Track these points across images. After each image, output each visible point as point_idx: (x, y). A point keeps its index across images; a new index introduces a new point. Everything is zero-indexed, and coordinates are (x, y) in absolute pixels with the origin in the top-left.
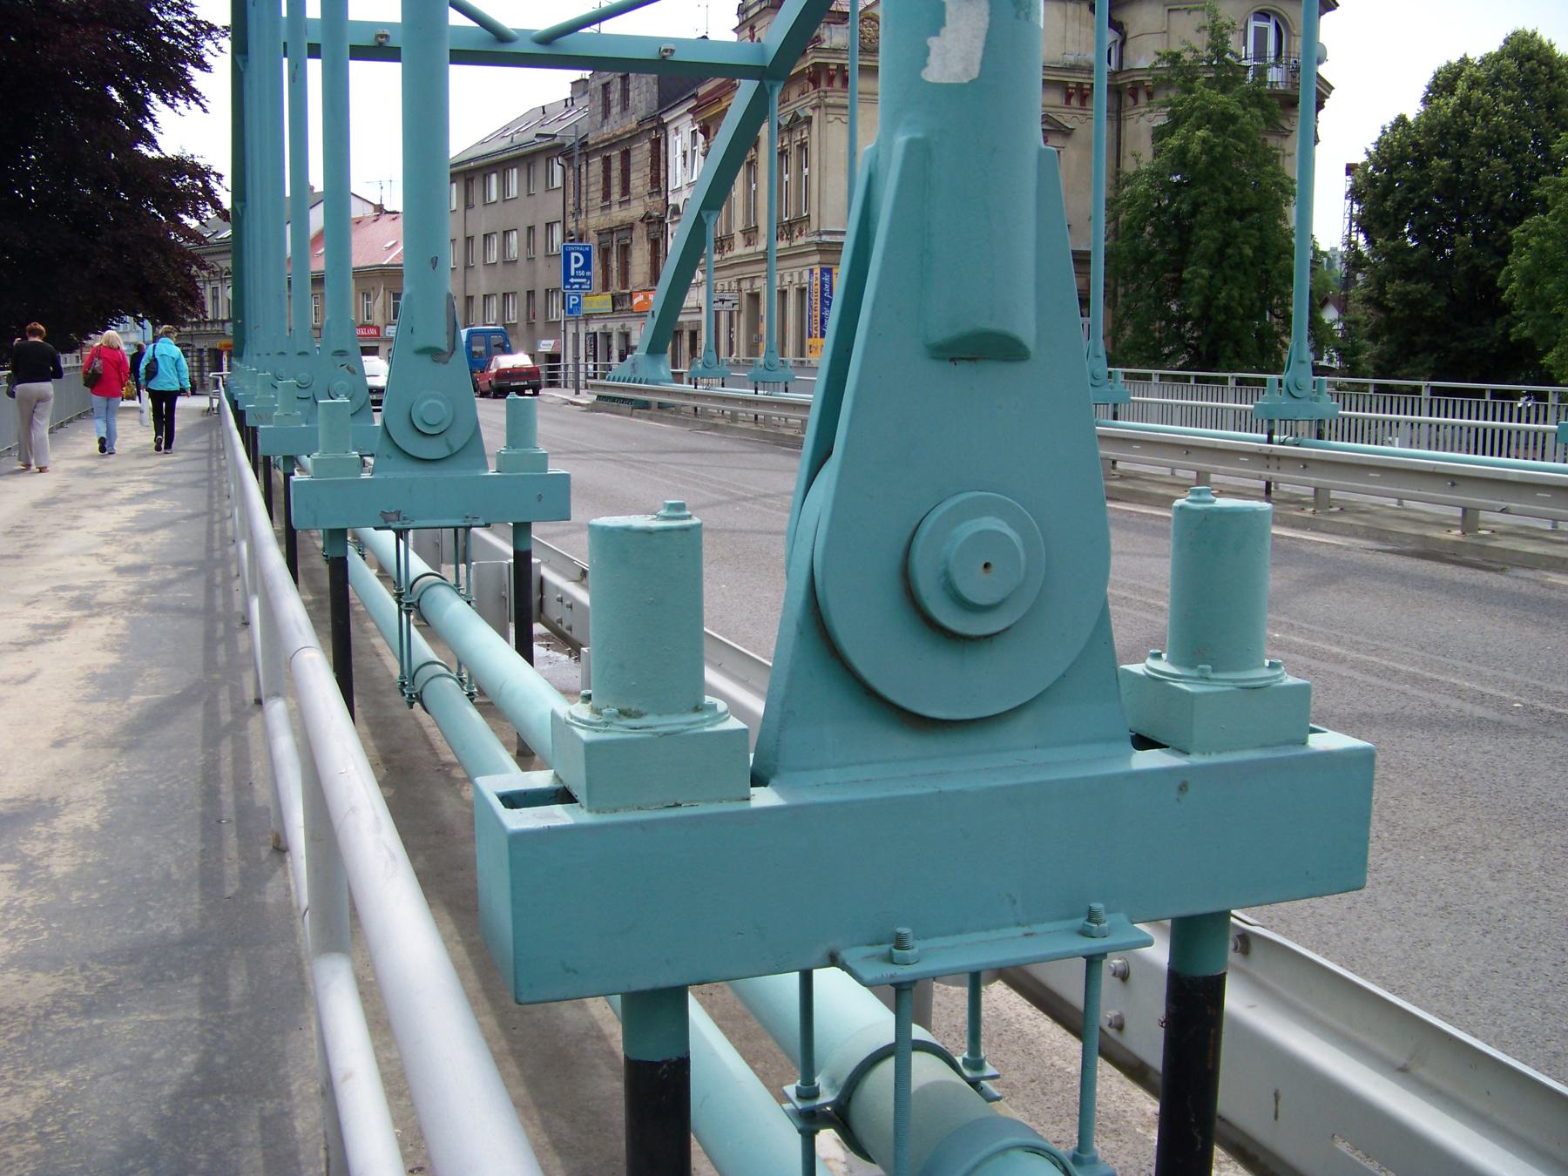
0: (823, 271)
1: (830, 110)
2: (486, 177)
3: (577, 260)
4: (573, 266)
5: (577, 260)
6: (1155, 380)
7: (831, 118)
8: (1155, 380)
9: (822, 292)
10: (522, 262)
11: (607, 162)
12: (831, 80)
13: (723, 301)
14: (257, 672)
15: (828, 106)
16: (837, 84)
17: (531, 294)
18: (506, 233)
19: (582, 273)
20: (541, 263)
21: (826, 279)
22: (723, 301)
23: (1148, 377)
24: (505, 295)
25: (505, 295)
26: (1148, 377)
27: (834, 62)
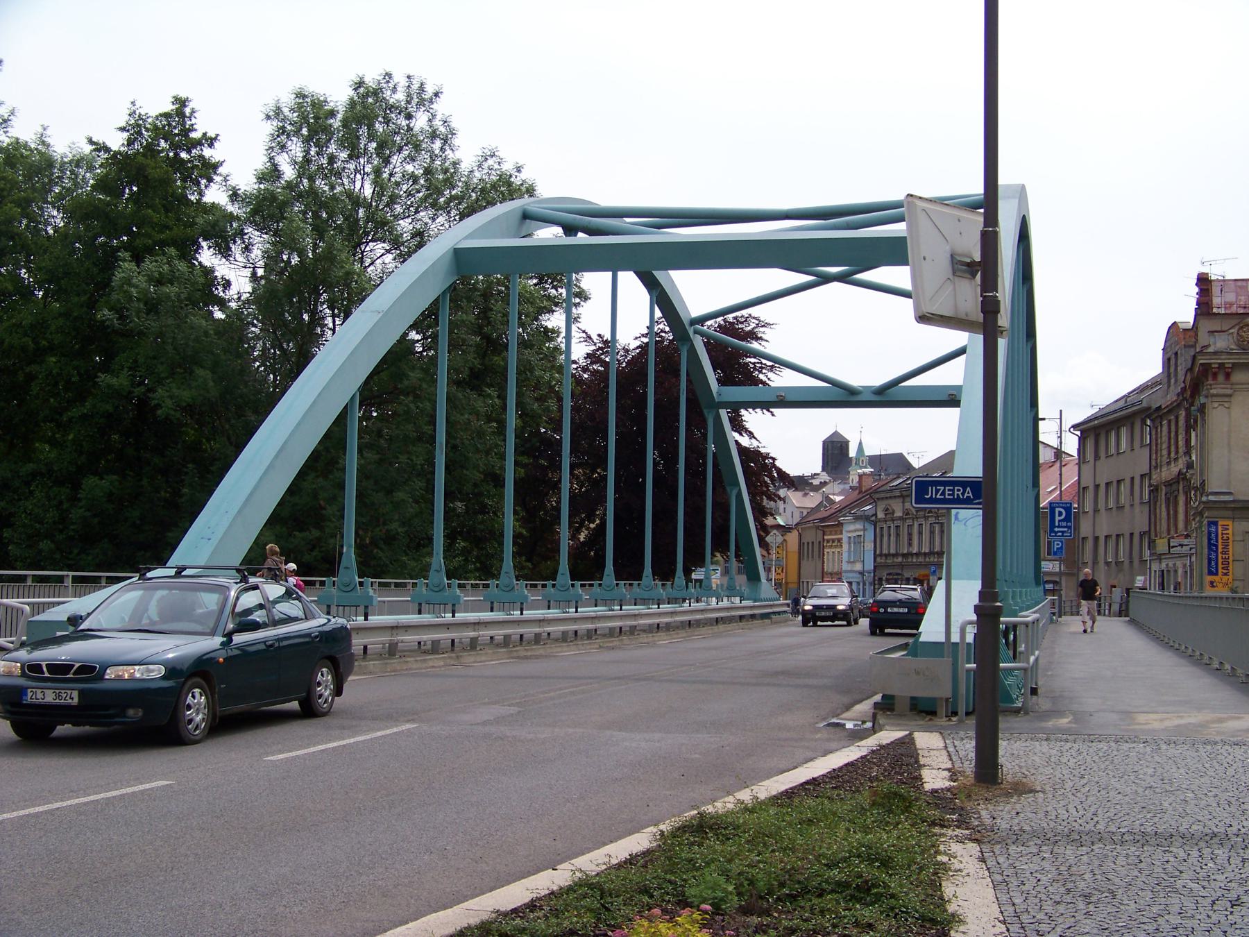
0: (1210, 524)
1: (1215, 399)
2: (1107, 433)
3: (1060, 514)
4: (1057, 518)
5: (1060, 514)
6: (469, 587)
7: (1216, 405)
8: (469, 587)
9: (1209, 539)
10: (1127, 508)
11: (1169, 422)
12: (1215, 376)
13: (1182, 546)
14: (296, 619)
15: (1214, 395)
16: (1221, 378)
17: (1132, 534)
18: (1119, 482)
19: (1064, 524)
20: (1137, 508)
21: (1213, 529)
22: (1182, 546)
23: (60, 579)
24: (1118, 536)
25: (1118, 536)
26: (60, 579)
27: (1215, 362)
